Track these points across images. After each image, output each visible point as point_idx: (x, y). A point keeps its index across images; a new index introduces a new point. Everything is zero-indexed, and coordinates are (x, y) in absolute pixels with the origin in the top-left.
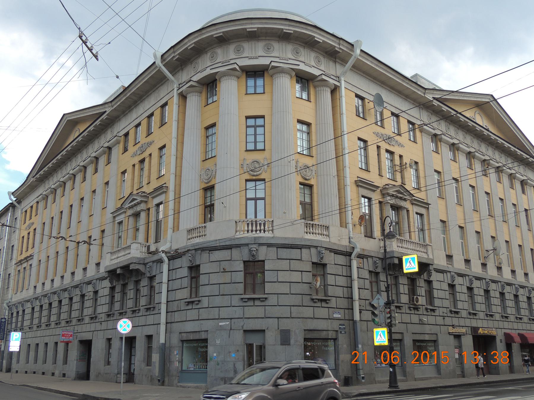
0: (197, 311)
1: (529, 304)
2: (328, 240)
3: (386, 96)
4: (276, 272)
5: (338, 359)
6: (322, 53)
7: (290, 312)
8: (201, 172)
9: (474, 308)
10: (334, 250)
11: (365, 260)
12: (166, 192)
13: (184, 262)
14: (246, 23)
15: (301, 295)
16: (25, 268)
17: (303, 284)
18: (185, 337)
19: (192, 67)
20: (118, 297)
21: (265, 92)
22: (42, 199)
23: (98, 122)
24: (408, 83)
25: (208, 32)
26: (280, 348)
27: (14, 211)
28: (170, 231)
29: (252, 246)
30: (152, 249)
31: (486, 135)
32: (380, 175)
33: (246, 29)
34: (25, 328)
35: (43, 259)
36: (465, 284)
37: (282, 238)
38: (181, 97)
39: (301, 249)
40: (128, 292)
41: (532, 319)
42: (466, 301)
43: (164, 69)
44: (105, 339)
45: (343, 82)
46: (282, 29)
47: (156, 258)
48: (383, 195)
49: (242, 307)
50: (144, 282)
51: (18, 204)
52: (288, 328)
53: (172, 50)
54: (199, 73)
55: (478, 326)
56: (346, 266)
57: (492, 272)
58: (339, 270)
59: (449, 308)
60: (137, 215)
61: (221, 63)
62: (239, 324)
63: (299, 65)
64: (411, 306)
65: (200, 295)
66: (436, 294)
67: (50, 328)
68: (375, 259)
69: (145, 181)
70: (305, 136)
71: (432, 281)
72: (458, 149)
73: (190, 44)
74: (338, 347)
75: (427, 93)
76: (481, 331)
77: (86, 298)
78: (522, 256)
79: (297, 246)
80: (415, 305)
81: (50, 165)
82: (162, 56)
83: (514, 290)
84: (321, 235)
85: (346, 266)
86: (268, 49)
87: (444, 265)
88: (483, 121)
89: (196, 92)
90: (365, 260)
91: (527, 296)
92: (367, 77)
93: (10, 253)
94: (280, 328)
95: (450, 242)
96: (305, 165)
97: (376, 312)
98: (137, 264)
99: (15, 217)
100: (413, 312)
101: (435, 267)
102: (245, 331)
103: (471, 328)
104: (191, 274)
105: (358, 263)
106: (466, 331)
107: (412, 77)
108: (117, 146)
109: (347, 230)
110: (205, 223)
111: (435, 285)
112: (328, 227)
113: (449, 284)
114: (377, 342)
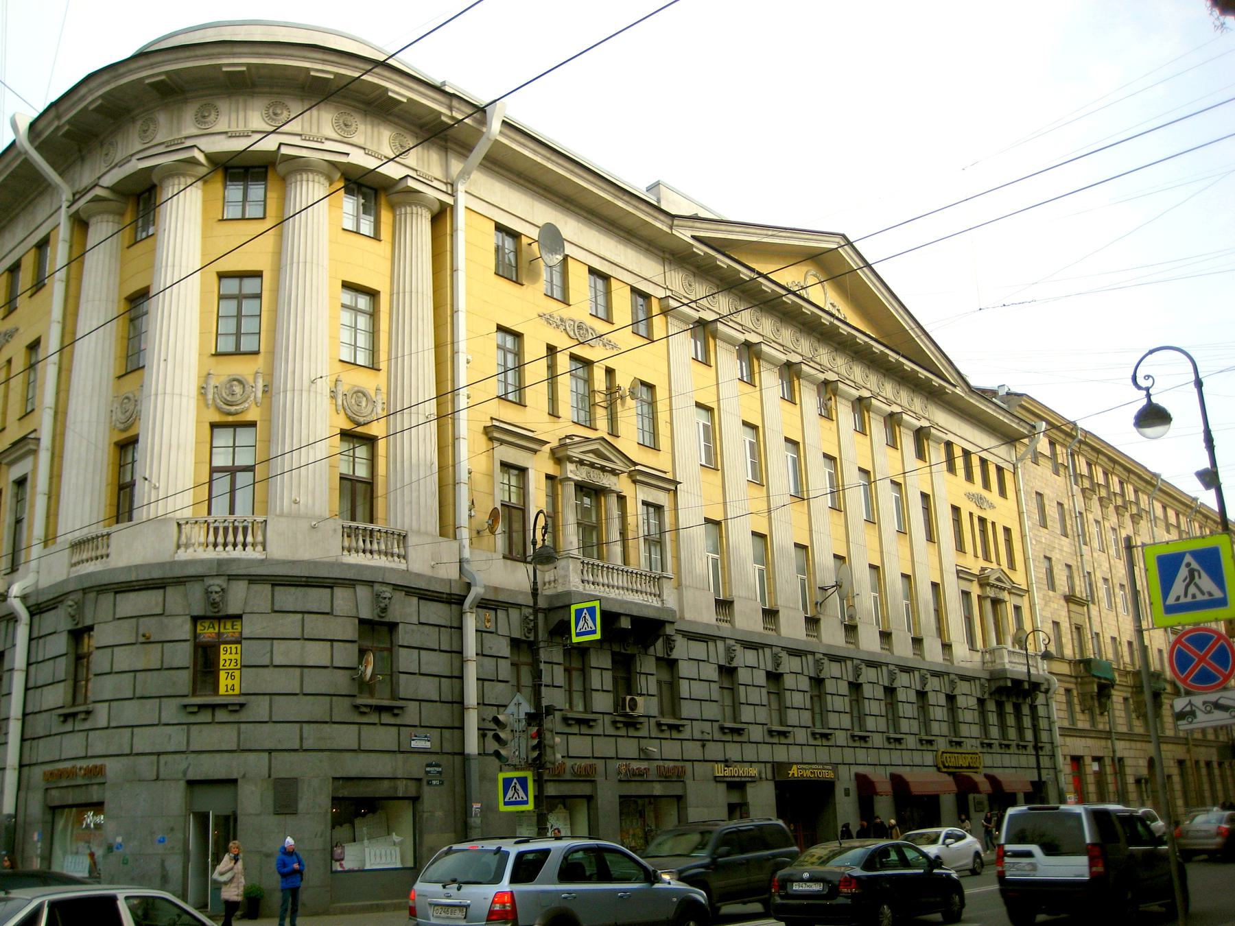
0: (82, 735)
1: (923, 707)
2: (403, 566)
3: (570, 228)
5: (421, 843)
7: (298, 737)
8: (112, 405)
9: (783, 720)
10: (417, 591)
13: (59, 621)
15: (328, 698)
17: (335, 670)
19: (104, 153)
24: (628, 202)
26: (271, 821)
31: (826, 325)
32: (554, 414)
36: (762, 666)
39: (332, 587)
41: (955, 742)
42: (762, 705)
46: (308, 70)
49: (185, 727)
52: (293, 775)
53: (53, 113)
55: (791, 761)
56: (451, 627)
58: (430, 638)
61: (163, 146)
62: (176, 766)
63: (348, 154)
64: (619, 719)
66: (684, 688)
70: (363, 322)
71: (677, 660)
74: (421, 817)
75: (677, 226)
76: (794, 772)
78: (911, 600)
79: (321, 580)
80: (626, 715)
85: (451, 627)
87: (710, 623)
90: (501, 614)
91: (918, 689)
92: (527, 184)
94: (274, 776)
95: (730, 571)
96: (356, 389)
97: (502, 735)
100: (623, 732)
101: (676, 626)
102: (191, 784)
103: (773, 766)
106: (760, 773)
109: (455, 544)
111: (685, 669)
112: (404, 537)
113: (721, 668)
114: (506, 804)
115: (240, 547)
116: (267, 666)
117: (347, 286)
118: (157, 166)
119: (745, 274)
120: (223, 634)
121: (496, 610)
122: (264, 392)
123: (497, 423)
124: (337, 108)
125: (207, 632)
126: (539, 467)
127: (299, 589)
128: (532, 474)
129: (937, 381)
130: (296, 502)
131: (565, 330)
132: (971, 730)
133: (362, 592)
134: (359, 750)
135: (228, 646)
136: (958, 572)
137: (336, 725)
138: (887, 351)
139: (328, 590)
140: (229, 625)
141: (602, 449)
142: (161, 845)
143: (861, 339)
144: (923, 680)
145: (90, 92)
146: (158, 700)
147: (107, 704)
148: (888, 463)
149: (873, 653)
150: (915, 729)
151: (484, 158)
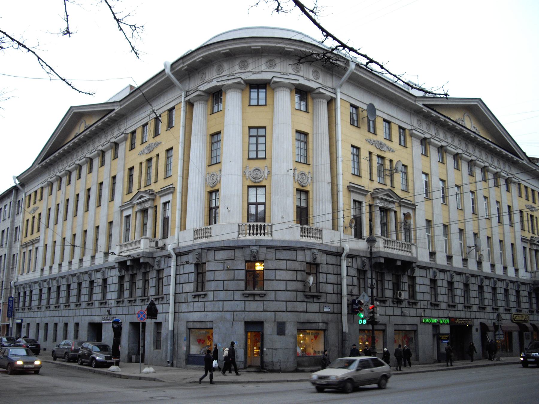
2: (321, 242)
3: (378, 104)
4: (274, 271)
6: (319, 67)
8: (206, 177)
12: (173, 192)
16: (30, 251)
18: (191, 325)
20: (127, 286)
21: (267, 104)
23: (106, 119)
25: (215, 48)
26: (277, 338)
28: (177, 230)
29: (253, 248)
30: (160, 244)
32: (371, 180)
33: (250, 47)
34: (33, 308)
35: (50, 243)
37: (279, 241)
38: (187, 107)
40: (137, 282)
43: (173, 77)
47: (164, 253)
48: (373, 198)
50: (152, 275)
52: (283, 321)
53: (181, 61)
57: (472, 266)
60: (145, 211)
64: (395, 300)
65: (206, 290)
66: (418, 288)
68: (363, 259)
69: (153, 180)
72: (446, 151)
77: (95, 284)
80: (398, 299)
81: (56, 154)
82: (172, 65)
89: (203, 100)
93: (14, 235)
99: (18, 200)
101: (418, 264)
108: (124, 142)
110: (210, 225)
111: (418, 280)
115: (262, 235)
117: (297, 131)
118: (224, 85)
119: (442, 118)
121: (352, 258)
123: (351, 185)
126: (366, 201)
128: (364, 204)
129: (516, 158)
132: (525, 305)
133: (308, 252)
136: (522, 239)
138: (496, 147)
139: (295, 252)
141: (389, 193)
143: (486, 142)
145: (198, 55)
147: (212, 292)
148: (494, 194)
149: (488, 273)
150: (503, 305)
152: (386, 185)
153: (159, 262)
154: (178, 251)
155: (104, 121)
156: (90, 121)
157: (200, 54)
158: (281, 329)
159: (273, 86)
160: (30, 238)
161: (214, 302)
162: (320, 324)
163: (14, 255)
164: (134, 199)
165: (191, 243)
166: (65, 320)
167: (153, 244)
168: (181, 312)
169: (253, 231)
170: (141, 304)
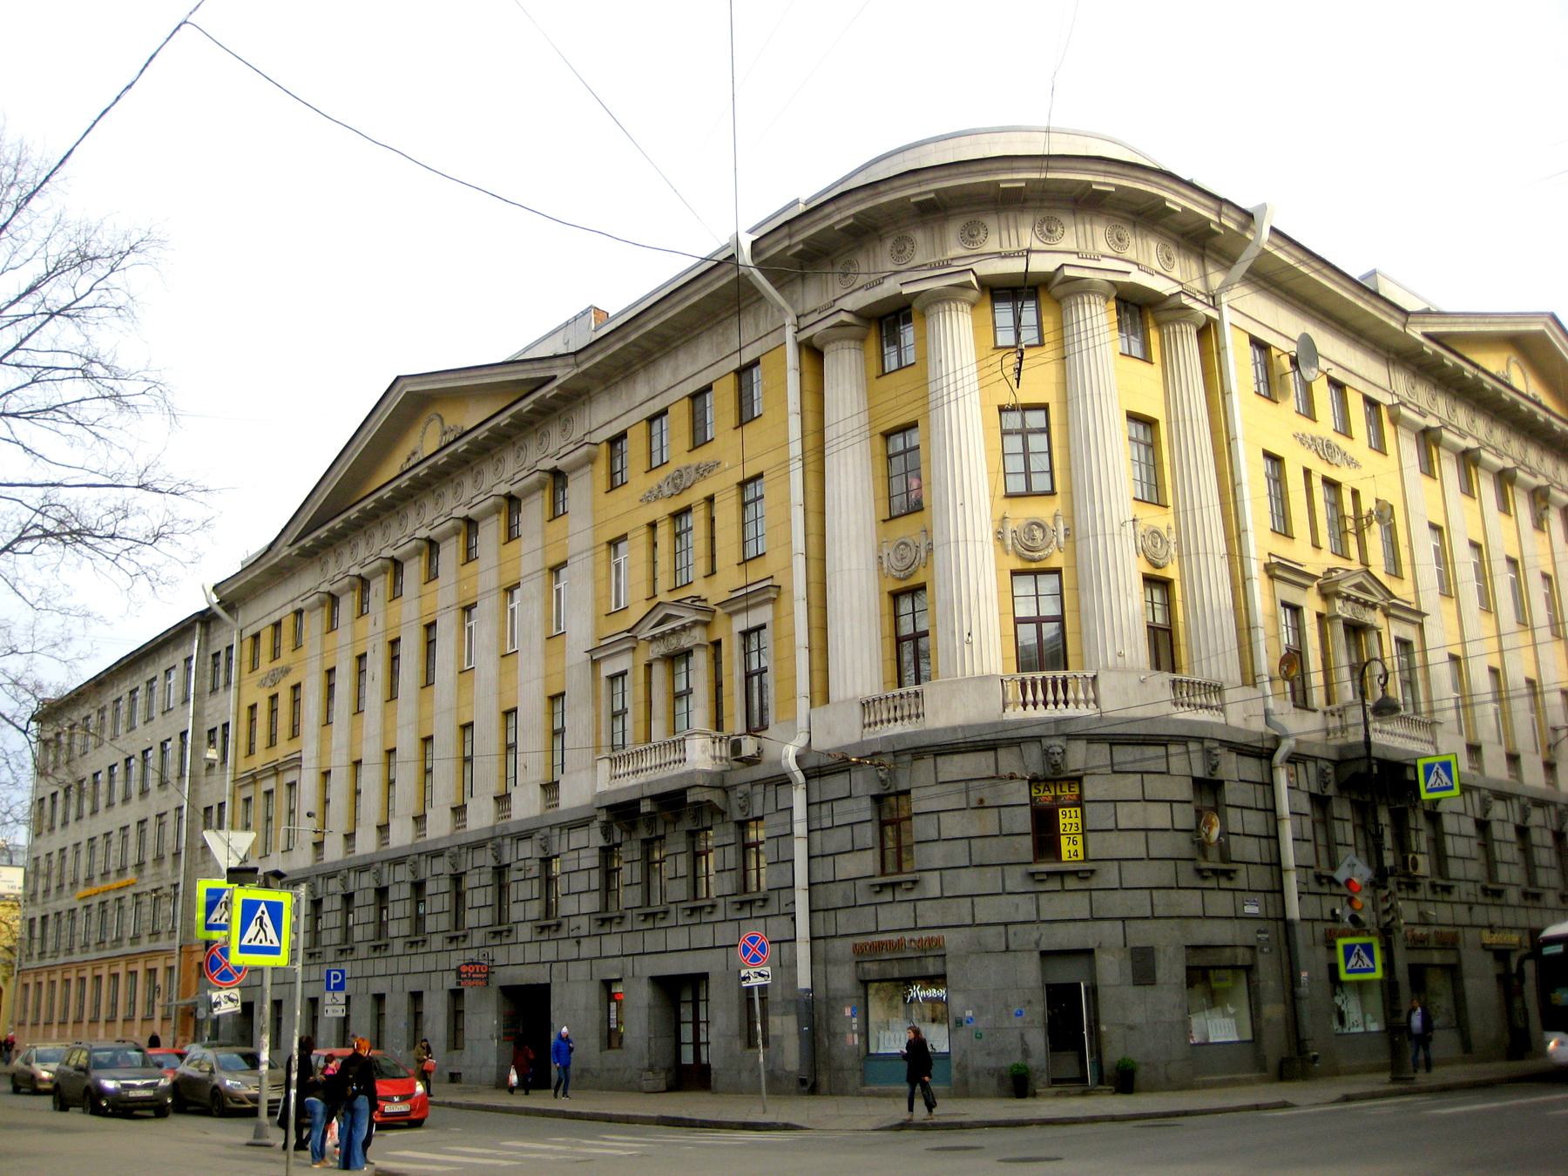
2: (1222, 720)
11: (1300, 767)
12: (775, 599)
14: (998, 169)
22: (318, 603)
26: (1132, 992)
27: (207, 634)
28: (803, 705)
33: (997, 183)
35: (340, 765)
44: (596, 984)
45: (1225, 308)
47: (758, 772)
49: (1033, 895)
51: (226, 611)
53: (785, 231)
54: (862, 292)
59: (1312, 867)
63: (1129, 273)
64: (1402, 880)
67: (388, 954)
68: (1321, 764)
73: (842, 216)
77: (513, 875)
78: (1538, 713)
80: (1408, 875)
83: (1477, 806)
84: (1207, 708)
86: (1050, 231)
88: (1527, 383)
89: (851, 338)
94: (1130, 945)
98: (706, 789)
102: (1045, 955)
104: (880, 812)
105: (1289, 775)
107: (1365, 277)
110: (900, 686)
115: (1041, 706)
116: (1112, 830)
119: (386, 493)
120: (1060, 796)
122: (1066, 536)
124: (1108, 221)
125: (1045, 795)
127: (1136, 748)
130: (1120, 655)
131: (1316, 450)
134: (1205, 917)
135: (1067, 810)
137: (1182, 891)
140: (1065, 788)
142: (1019, 1018)
144: (1525, 813)
146: (999, 868)
151: (1248, 271)
152: (1350, 559)
153: (747, 797)
154: (811, 762)
155: (520, 410)
156: (470, 417)
157: (848, 207)
158: (1143, 967)
159: (1058, 291)
160: (261, 759)
161: (943, 901)
162: (1240, 951)
163: (208, 809)
164: (642, 625)
165: (856, 738)
166: (413, 984)
167: (725, 751)
168: (835, 936)
169: (1045, 694)
170: (689, 921)
